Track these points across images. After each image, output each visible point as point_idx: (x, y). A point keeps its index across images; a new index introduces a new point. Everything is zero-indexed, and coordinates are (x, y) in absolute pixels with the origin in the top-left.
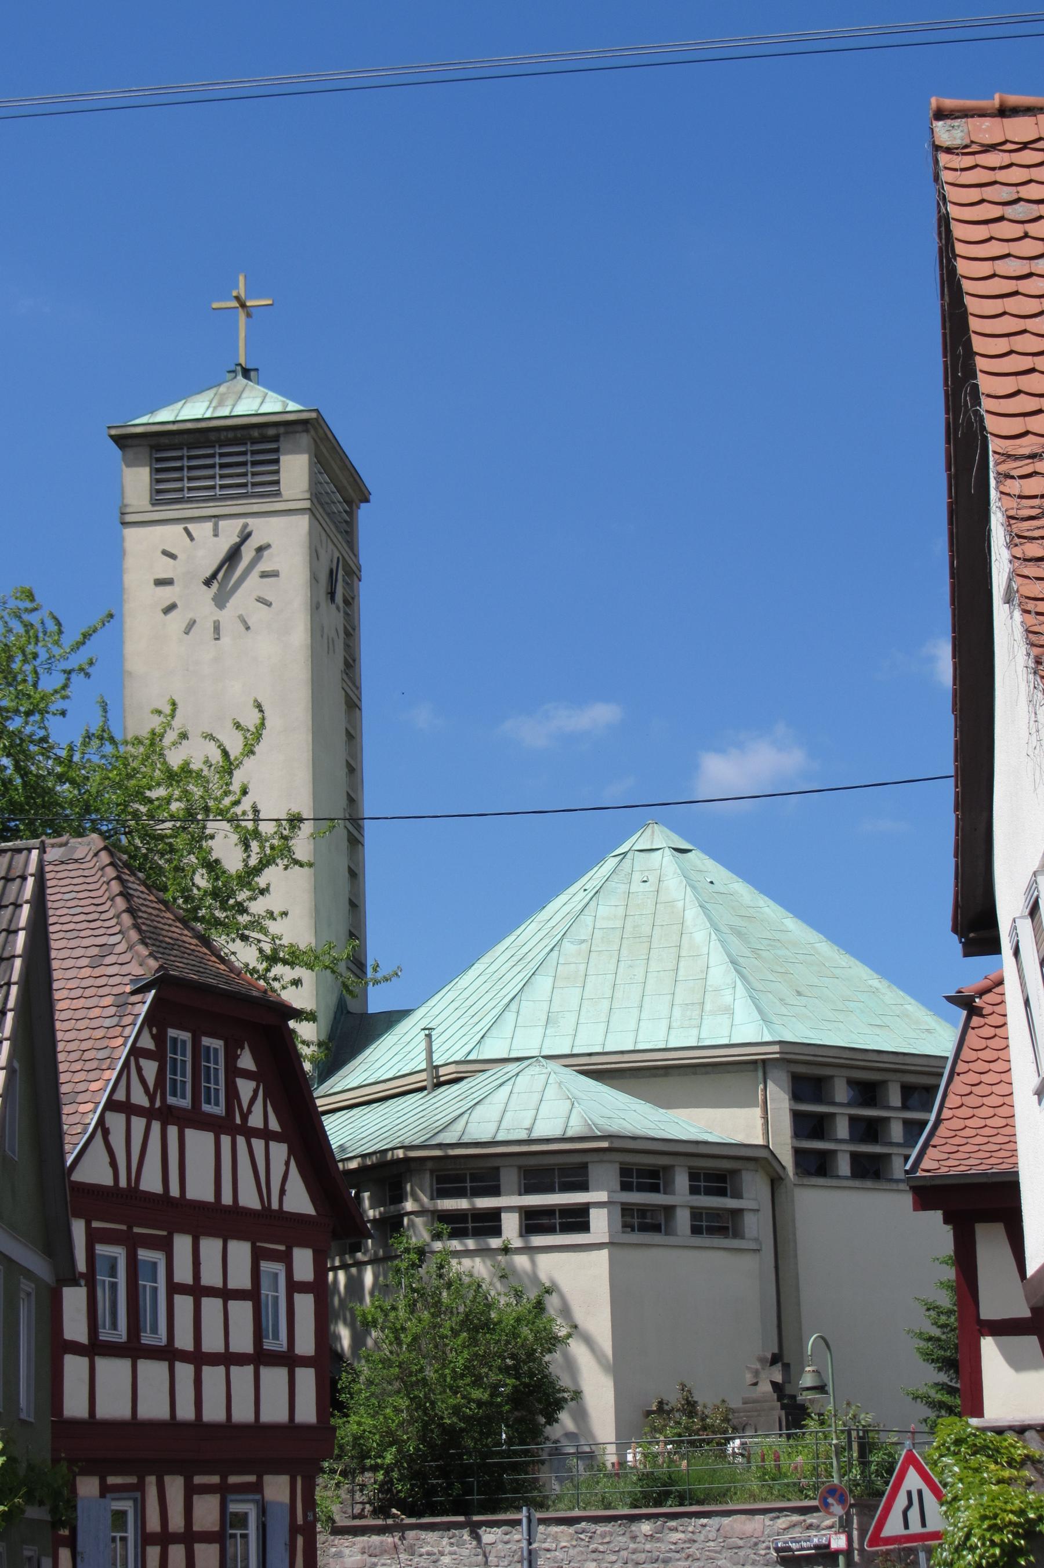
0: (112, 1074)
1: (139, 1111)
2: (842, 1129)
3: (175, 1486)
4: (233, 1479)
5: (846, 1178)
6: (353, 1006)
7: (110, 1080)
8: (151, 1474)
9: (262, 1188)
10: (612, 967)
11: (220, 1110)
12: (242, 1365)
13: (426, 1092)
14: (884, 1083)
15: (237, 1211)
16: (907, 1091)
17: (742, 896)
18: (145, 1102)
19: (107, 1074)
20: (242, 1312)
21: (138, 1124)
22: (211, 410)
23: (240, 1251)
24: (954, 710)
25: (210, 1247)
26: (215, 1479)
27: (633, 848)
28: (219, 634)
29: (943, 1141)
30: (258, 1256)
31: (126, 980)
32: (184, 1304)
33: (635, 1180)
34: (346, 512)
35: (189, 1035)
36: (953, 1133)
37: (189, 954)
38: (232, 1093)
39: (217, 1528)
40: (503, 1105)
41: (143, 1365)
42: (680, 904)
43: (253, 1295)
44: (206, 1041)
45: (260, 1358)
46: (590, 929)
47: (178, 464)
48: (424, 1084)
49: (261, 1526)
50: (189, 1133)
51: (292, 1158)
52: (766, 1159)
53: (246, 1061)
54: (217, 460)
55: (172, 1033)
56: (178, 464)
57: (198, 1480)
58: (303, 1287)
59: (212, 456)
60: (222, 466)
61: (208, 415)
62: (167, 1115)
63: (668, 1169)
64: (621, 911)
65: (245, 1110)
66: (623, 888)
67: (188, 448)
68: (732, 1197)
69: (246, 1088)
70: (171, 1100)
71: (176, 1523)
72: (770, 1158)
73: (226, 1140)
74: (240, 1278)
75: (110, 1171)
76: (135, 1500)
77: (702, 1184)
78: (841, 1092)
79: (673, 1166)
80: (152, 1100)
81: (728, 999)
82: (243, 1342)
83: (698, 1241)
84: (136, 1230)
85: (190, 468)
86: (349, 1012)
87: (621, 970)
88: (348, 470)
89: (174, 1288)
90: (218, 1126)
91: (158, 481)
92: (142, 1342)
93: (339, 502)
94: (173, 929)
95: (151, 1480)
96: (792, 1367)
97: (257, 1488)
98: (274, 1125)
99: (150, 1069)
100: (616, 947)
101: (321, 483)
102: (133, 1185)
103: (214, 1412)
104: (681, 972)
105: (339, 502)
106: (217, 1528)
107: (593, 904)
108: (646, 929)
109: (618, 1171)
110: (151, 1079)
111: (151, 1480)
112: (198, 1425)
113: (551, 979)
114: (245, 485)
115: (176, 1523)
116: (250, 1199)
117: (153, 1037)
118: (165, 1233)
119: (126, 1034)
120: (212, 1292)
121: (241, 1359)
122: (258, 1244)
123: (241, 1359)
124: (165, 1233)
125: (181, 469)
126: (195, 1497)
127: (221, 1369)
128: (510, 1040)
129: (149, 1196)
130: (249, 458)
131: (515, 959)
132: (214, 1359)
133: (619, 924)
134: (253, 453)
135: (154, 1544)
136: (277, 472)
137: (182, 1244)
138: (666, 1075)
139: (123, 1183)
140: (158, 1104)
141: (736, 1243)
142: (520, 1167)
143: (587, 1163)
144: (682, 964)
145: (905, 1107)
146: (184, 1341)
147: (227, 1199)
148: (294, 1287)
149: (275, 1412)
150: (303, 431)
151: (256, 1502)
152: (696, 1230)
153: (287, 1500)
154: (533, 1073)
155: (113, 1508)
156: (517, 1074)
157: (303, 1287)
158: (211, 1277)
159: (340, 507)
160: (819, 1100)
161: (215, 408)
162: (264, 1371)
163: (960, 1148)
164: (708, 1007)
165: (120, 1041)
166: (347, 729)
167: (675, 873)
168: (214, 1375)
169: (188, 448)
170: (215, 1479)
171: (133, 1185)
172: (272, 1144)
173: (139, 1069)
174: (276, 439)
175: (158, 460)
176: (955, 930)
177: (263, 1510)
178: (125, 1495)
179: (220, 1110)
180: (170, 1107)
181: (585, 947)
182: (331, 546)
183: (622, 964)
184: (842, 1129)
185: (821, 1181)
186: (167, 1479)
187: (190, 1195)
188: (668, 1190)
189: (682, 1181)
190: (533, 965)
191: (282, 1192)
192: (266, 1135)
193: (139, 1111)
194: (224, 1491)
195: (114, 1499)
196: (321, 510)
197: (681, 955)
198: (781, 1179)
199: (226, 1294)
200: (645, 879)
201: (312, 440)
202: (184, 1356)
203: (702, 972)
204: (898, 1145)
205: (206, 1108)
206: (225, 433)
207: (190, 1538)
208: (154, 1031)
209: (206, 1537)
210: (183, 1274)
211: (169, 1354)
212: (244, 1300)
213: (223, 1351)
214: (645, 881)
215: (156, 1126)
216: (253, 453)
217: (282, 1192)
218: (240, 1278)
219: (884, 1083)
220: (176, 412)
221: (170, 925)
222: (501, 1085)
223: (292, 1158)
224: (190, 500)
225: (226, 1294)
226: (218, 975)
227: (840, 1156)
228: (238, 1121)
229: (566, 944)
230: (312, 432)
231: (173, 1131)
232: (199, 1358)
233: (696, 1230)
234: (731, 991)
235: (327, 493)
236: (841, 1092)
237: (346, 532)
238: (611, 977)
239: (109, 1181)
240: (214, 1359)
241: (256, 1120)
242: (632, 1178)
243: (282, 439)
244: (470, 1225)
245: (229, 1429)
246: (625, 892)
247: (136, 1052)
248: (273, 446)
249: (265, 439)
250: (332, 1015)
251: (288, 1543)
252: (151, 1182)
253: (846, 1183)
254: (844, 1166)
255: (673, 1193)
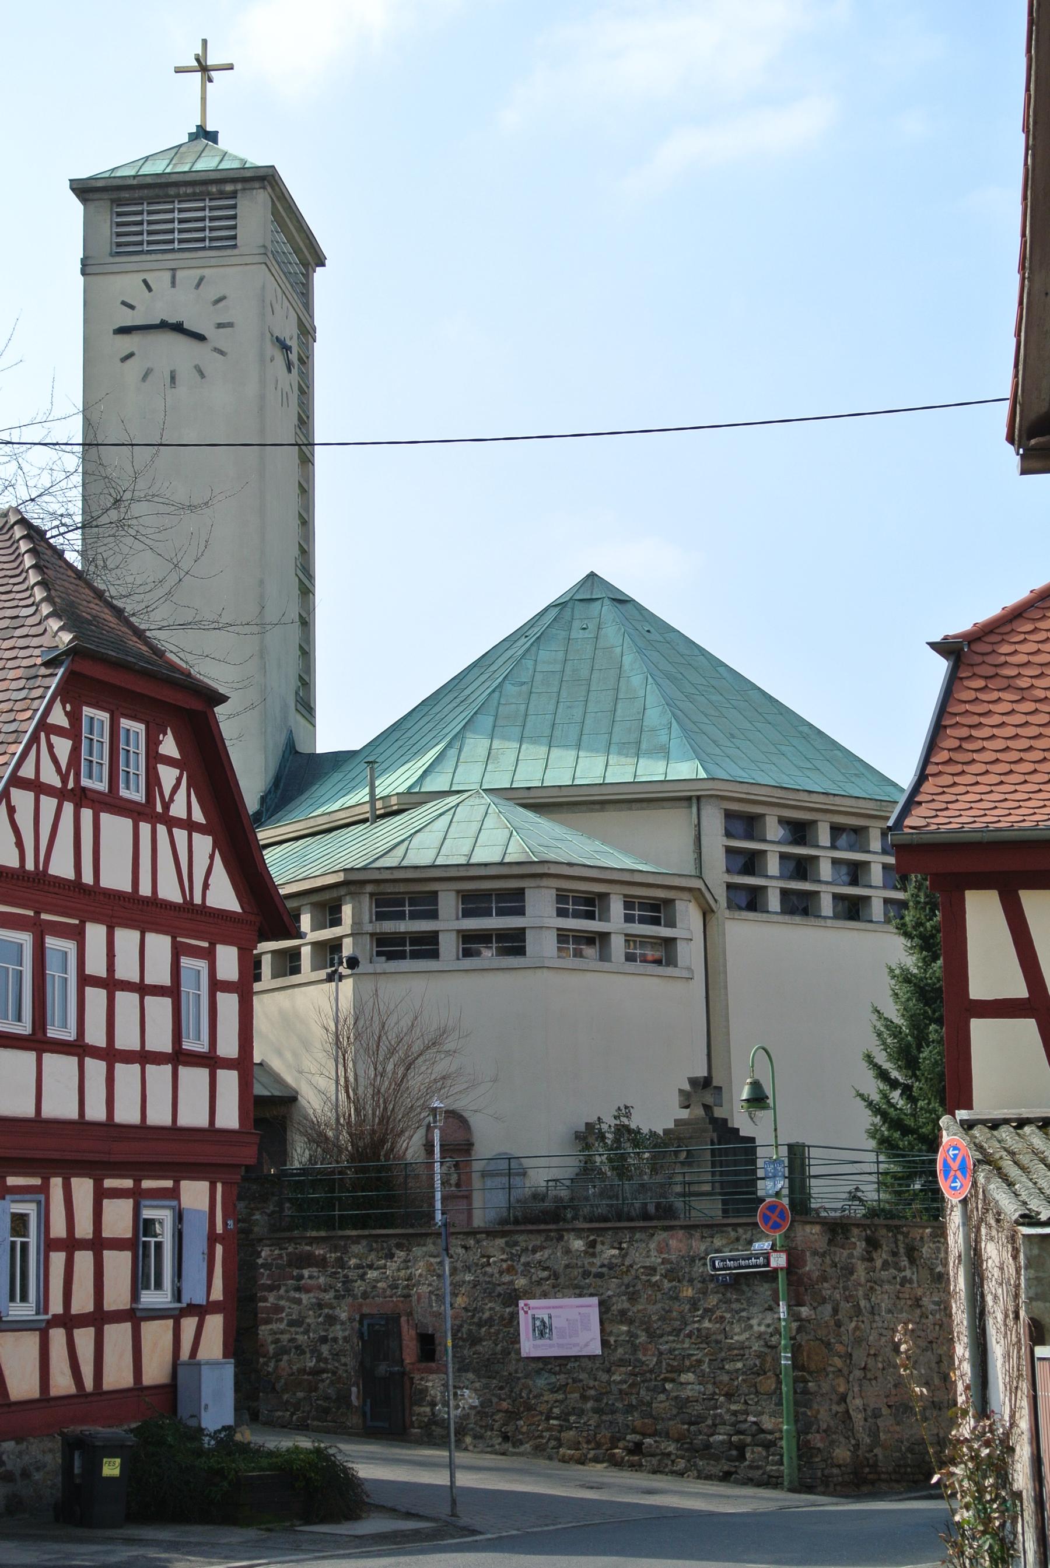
0: (18, 748)
1: (50, 791)
2: (773, 866)
3: (83, 1188)
4: (147, 1184)
5: (776, 913)
6: (303, 748)
7: (15, 754)
8: (56, 1175)
9: (184, 880)
10: (551, 707)
11: (140, 797)
12: (159, 1064)
13: (368, 824)
14: (814, 823)
15: (155, 902)
16: (836, 830)
17: (678, 644)
18: (57, 782)
19: (12, 748)
20: (160, 1008)
21: (48, 804)
22: (171, 166)
23: (160, 945)
24: (1026, 129)
25: (127, 939)
26: (128, 1183)
27: (576, 597)
28: (174, 383)
29: (930, 798)
30: (178, 952)
31: (37, 652)
32: (96, 997)
33: (571, 907)
34: (303, 274)
35: (107, 715)
36: (940, 790)
37: (108, 632)
38: (153, 781)
39: (129, 1235)
40: (442, 834)
41: (50, 1059)
42: (618, 650)
43: (173, 991)
44: (125, 723)
45: (179, 1057)
46: (531, 672)
47: (138, 218)
48: (368, 815)
49: (177, 1233)
50: (104, 817)
51: (217, 851)
52: (699, 889)
53: (169, 746)
54: (176, 215)
55: (87, 711)
56: (138, 218)
57: (109, 1183)
58: (227, 987)
59: (172, 211)
60: (181, 221)
61: (168, 170)
62: (81, 797)
63: (604, 897)
64: (561, 655)
65: (167, 799)
66: (563, 634)
67: (149, 203)
68: (666, 926)
69: (168, 775)
70: (85, 782)
71: (84, 1229)
72: (704, 889)
73: (145, 828)
74: (159, 974)
75: (16, 852)
76: (39, 1203)
77: (637, 913)
78: (774, 831)
79: (608, 894)
80: (64, 780)
81: (664, 739)
82: (160, 1041)
83: (631, 967)
84: (44, 916)
85: (150, 223)
86: (297, 752)
87: (560, 710)
88: (305, 231)
89: (85, 980)
90: (137, 813)
91: (119, 235)
92: (49, 1035)
93: (296, 264)
94: (92, 605)
95: (56, 1183)
96: (723, 1089)
97: (174, 1194)
98: (198, 816)
99: (63, 747)
100: (555, 689)
101: (277, 242)
102: (41, 869)
103: (127, 1114)
104: (619, 712)
105: (296, 264)
106: (129, 1235)
107: (534, 649)
108: (585, 673)
109: (555, 896)
110: (63, 756)
111: (56, 1183)
112: (110, 1127)
113: (492, 719)
114: (203, 240)
115: (84, 1229)
116: (170, 891)
117: (67, 714)
118: (77, 922)
119: (34, 707)
120: (127, 986)
121: (158, 1058)
122: (178, 939)
123: (158, 1058)
124: (77, 922)
125: (141, 223)
126: (106, 1202)
127: (137, 1067)
128: (451, 775)
129: (59, 882)
130: (207, 213)
131: (458, 700)
132: (128, 1057)
133: (558, 667)
134: (212, 209)
135: (58, 1249)
136: (234, 227)
137: (95, 933)
138: (602, 810)
139: (30, 866)
140: (71, 785)
141: (669, 971)
142: (458, 892)
143: (523, 889)
144: (619, 706)
145: (833, 847)
146: (96, 1036)
147: (145, 890)
148: (216, 986)
149: (193, 1116)
150: (260, 188)
151: (173, 1208)
152: (630, 958)
153: (205, 1207)
154: (472, 804)
155: (12, 1211)
156: (458, 805)
157: (227, 987)
158: (127, 970)
159: (298, 269)
160: (750, 837)
161: (175, 165)
162: (183, 1071)
163: (949, 806)
164: (644, 746)
165: (29, 714)
166: (299, 482)
167: (614, 620)
168: (127, 1074)
169: (149, 203)
170: (128, 1183)
171: (41, 869)
172: (195, 835)
173: (50, 747)
174: (234, 195)
175: (119, 214)
176: (1010, 439)
177: (179, 1216)
178: (28, 1197)
179: (140, 797)
180: (84, 790)
181: (524, 688)
182: (286, 303)
183: (561, 705)
184: (773, 866)
185: (751, 915)
186: (74, 1181)
187: (105, 883)
188: (605, 917)
189: (617, 908)
190: (475, 707)
191: (206, 886)
192: (190, 826)
193: (50, 791)
194: (137, 1195)
195: (13, 1201)
196: (277, 266)
197: (619, 697)
198: (713, 911)
199: (143, 989)
200: (584, 626)
201: (268, 196)
202: (95, 1052)
203: (639, 713)
204: (827, 883)
205: (124, 793)
206: (184, 189)
207: (98, 1244)
208: (68, 707)
209: (117, 1244)
210: (96, 966)
211: (79, 1049)
212: (163, 995)
213: (139, 1049)
214: (584, 629)
215: (68, 808)
216: (212, 209)
217: (206, 886)
218: (159, 974)
219: (814, 823)
220: (137, 168)
221: (89, 602)
222: (441, 815)
223: (217, 851)
224: (149, 252)
225: (143, 989)
226: (141, 656)
227: (770, 891)
228: (159, 809)
229: (508, 687)
230: (269, 189)
231: (87, 814)
232: (111, 1055)
233: (630, 958)
234: (666, 731)
235: (284, 253)
236: (774, 831)
237: (303, 294)
238: (549, 717)
239: (15, 863)
240: (128, 1057)
241: (178, 810)
242: (568, 905)
243: (239, 195)
244: (408, 948)
245: (143, 1131)
246: (565, 639)
247: (43, 726)
248: (231, 202)
249: (222, 195)
250: (280, 753)
251: (206, 1251)
252: (61, 867)
253: (775, 918)
254: (774, 902)
255: (608, 920)
